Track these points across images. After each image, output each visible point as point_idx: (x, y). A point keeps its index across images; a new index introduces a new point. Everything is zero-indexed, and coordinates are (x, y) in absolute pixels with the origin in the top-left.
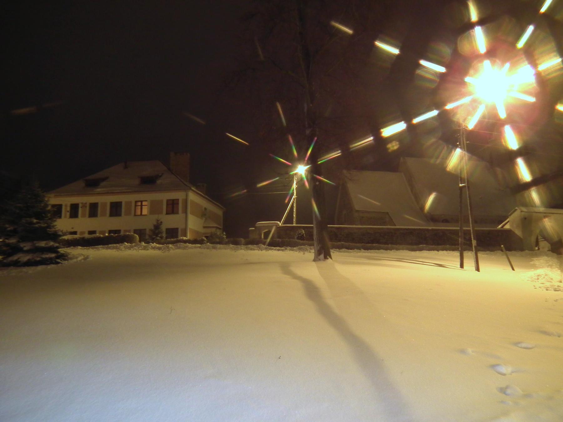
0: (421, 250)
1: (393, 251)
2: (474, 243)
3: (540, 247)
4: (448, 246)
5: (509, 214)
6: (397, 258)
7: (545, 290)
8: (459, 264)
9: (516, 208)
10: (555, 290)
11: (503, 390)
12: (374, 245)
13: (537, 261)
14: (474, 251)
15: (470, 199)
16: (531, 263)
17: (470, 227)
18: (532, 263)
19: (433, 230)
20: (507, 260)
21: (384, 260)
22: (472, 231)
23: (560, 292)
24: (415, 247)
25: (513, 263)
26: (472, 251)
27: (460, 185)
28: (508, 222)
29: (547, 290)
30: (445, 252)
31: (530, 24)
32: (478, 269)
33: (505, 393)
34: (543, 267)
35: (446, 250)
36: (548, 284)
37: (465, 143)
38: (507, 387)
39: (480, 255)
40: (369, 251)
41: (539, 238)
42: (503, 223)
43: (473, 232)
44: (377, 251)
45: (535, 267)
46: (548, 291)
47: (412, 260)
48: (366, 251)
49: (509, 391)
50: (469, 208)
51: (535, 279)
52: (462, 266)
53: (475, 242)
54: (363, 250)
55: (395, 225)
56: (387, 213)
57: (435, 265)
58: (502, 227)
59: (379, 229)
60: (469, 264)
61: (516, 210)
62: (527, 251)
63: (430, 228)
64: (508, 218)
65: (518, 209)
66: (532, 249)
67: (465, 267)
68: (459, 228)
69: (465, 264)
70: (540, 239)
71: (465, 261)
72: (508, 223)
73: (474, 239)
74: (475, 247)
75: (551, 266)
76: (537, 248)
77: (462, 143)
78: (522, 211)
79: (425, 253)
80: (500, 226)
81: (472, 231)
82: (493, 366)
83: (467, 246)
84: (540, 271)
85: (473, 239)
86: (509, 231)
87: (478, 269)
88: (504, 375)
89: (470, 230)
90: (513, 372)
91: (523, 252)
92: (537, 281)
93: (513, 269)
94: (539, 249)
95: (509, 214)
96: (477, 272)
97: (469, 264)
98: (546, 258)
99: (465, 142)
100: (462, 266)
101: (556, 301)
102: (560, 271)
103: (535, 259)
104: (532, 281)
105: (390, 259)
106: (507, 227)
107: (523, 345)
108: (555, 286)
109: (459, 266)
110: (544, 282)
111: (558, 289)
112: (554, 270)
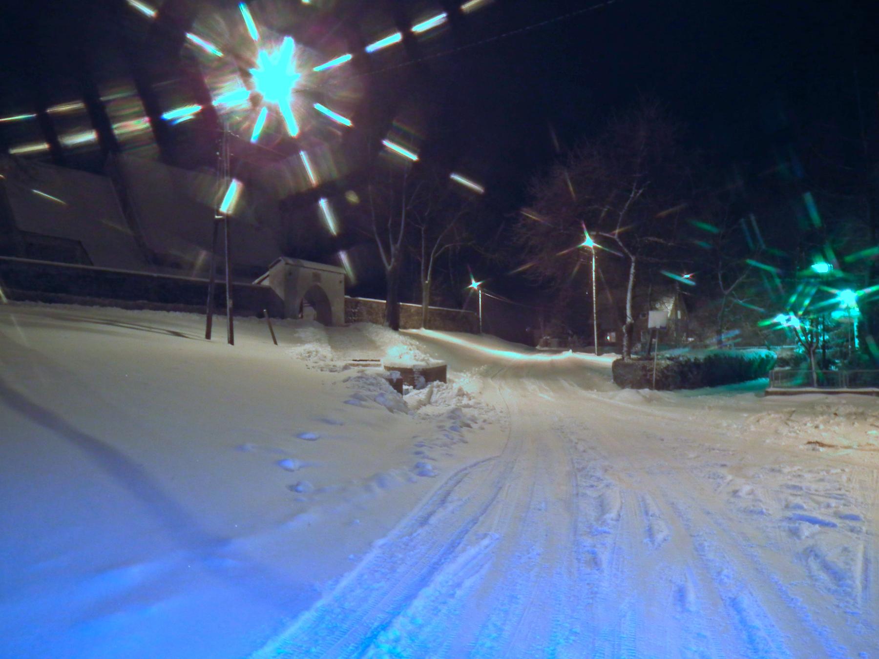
0: (140, 308)
1: (95, 307)
2: (229, 303)
3: (303, 315)
4: (182, 305)
5: (270, 265)
6: (107, 320)
7: (319, 371)
8: (204, 333)
9: (280, 258)
10: (331, 371)
11: (294, 488)
12: (60, 295)
13: (302, 333)
14: (228, 316)
15: (229, 241)
16: (295, 335)
17: (225, 280)
18: (296, 335)
19: (158, 278)
20: (268, 330)
21: (85, 321)
22: (227, 286)
23: (336, 373)
24: (131, 303)
25: (276, 335)
26: (225, 314)
27: (216, 217)
28: (268, 276)
29: (322, 370)
30: (178, 314)
31: (420, 156)
32: (231, 341)
33: (297, 491)
34: (310, 342)
35: (180, 310)
36: (322, 363)
37: (228, 156)
38: (298, 485)
39: (215, 318)
40: (53, 305)
41: (304, 302)
42: (261, 278)
43: (229, 287)
44: (68, 306)
45: (300, 341)
46: (323, 372)
47: (133, 324)
48: (48, 304)
49: (300, 488)
50: (226, 252)
51: (306, 357)
52: (208, 336)
53: (231, 302)
54: (41, 303)
55: (92, 264)
56: (79, 243)
57: (102, 321)
58: (260, 282)
59: (68, 268)
60: (220, 335)
61: (279, 261)
62: (289, 319)
63: (155, 275)
64: (267, 270)
65: (282, 259)
66: (295, 317)
67: (212, 338)
68: (207, 280)
69: (213, 334)
70: (305, 303)
71: (213, 329)
72: (268, 278)
73: (230, 298)
74: (230, 310)
75: (319, 341)
76: (300, 316)
77: (224, 154)
78: (287, 264)
79: (148, 314)
80: (257, 281)
81: (227, 286)
82: (279, 463)
83: (219, 307)
84: (309, 347)
85: (228, 298)
86: (268, 290)
87: (231, 341)
88: (292, 471)
89: (225, 285)
90: (300, 467)
91: (284, 320)
92: (308, 359)
93: (276, 343)
94: (302, 317)
95: (270, 265)
96: (230, 345)
97: (220, 335)
98: (311, 329)
99: (228, 154)
100: (208, 336)
101: (334, 383)
102: (329, 347)
103: (300, 330)
104: (303, 359)
105: (159, 331)
106: (266, 283)
107: (307, 436)
108: (330, 365)
109: (204, 336)
110: (317, 361)
111: (334, 370)
112: (323, 345)
